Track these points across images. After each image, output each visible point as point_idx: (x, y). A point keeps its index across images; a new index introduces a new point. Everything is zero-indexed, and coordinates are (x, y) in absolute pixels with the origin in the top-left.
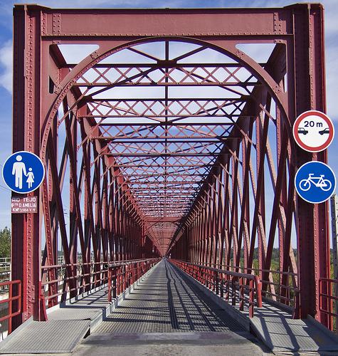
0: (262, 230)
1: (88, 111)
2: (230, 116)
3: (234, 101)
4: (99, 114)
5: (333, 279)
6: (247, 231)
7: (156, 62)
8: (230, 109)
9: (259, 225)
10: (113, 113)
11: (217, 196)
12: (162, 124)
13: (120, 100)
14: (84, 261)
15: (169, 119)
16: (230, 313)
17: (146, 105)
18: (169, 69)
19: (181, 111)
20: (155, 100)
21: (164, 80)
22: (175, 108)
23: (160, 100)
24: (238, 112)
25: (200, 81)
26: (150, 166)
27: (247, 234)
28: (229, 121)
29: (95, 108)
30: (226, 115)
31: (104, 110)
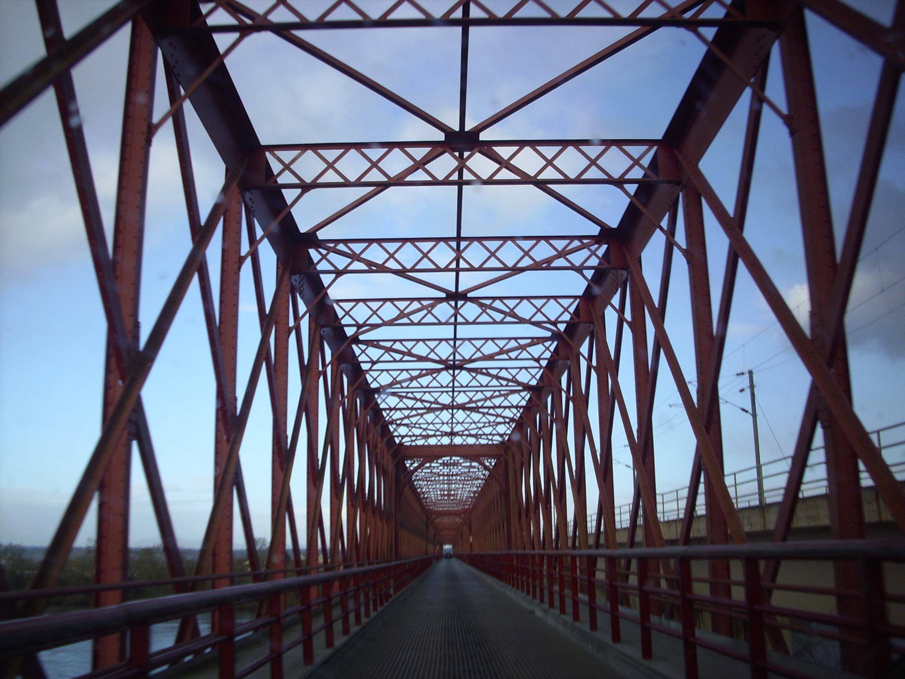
2: (537, 360)
10: (387, 357)
13: (370, 241)
20: (438, 240)
23: (446, 240)
24: (594, 262)
28: (536, 364)
29: (363, 351)
30: (534, 359)
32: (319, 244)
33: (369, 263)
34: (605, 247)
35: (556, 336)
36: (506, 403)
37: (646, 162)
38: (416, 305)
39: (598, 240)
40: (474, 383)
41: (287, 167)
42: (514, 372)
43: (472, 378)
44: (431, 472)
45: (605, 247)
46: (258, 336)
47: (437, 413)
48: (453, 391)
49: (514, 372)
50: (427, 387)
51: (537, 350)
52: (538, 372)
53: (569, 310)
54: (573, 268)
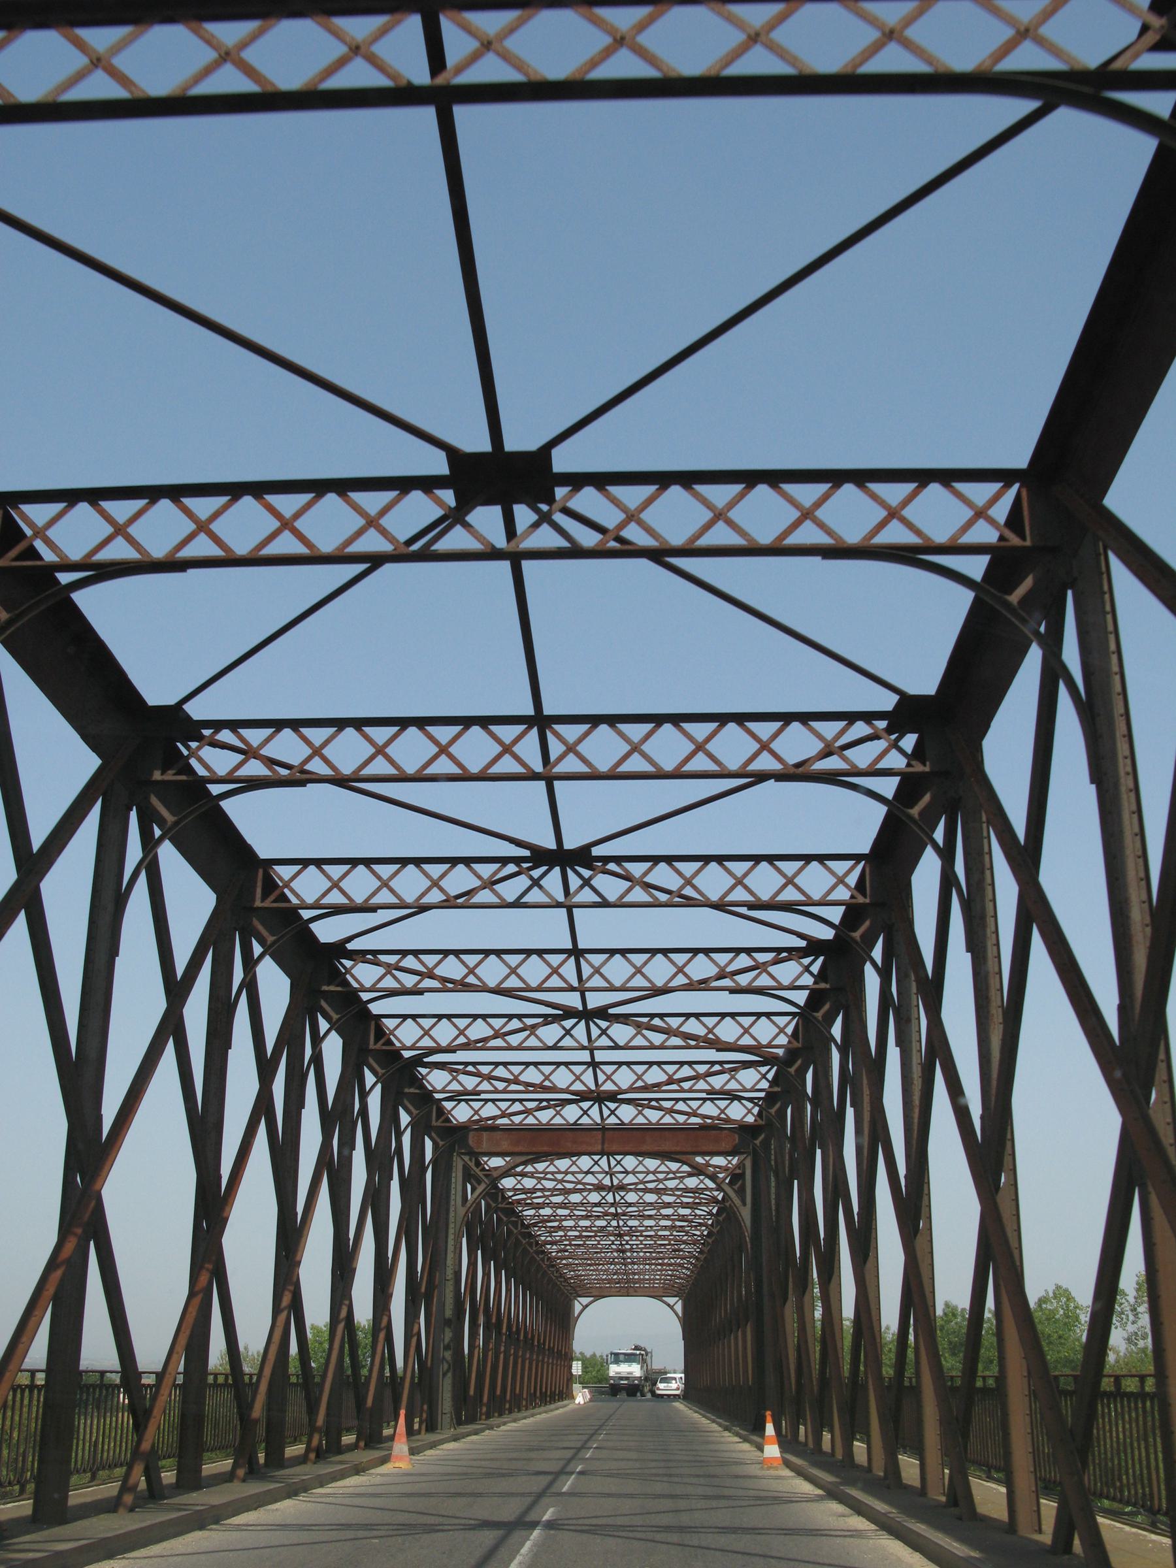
3: (783, 954)
13: (446, 953)
17: (456, 1026)
25: (664, 897)
32: (360, 956)
33: (444, 980)
37: (852, 880)
38: (515, 1024)
42: (639, 1041)
43: (638, 1162)
44: (565, 1236)
46: (319, 1138)
49: (639, 1041)
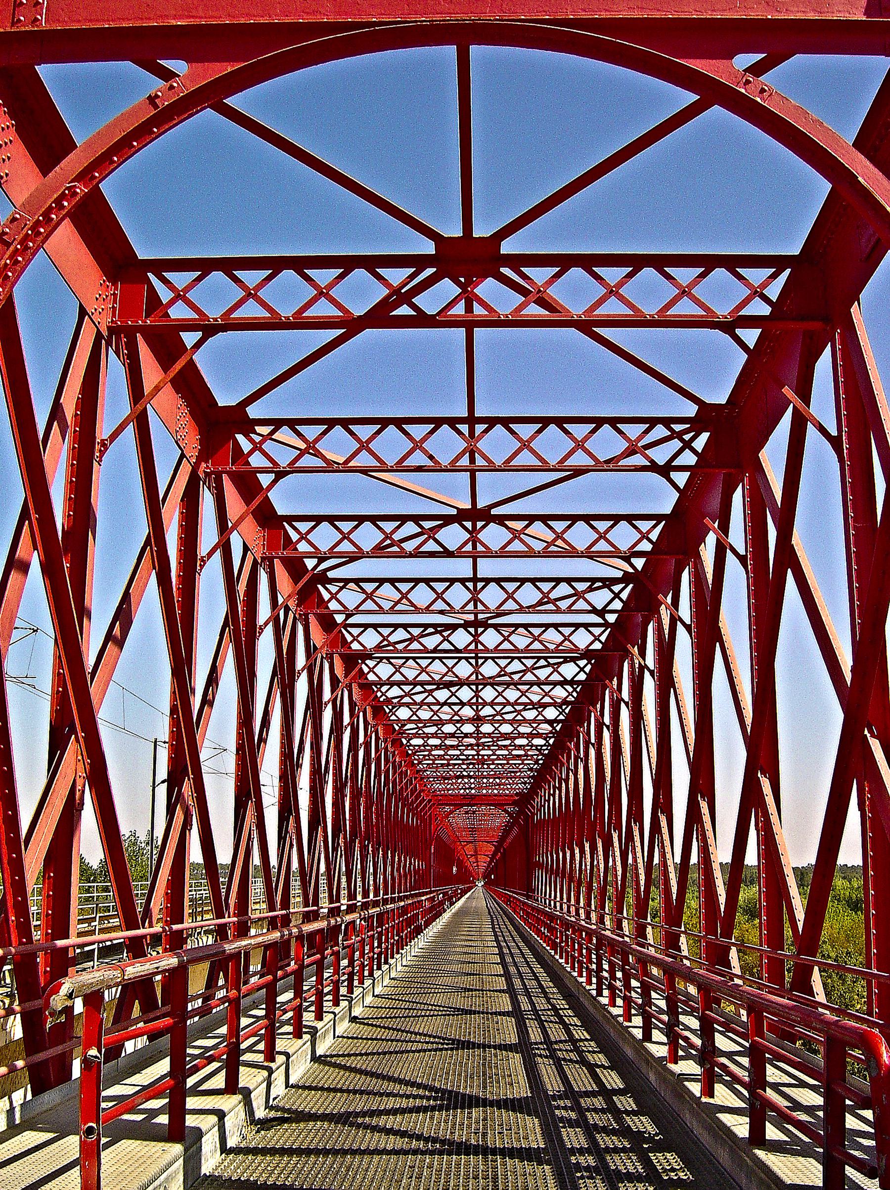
0: (667, 843)
1: (323, 603)
2: (601, 613)
3: (608, 583)
4: (340, 608)
5: (609, 928)
6: (638, 843)
7: (454, 512)
8: (600, 598)
9: (633, 840)
11: (592, 752)
12: (466, 625)
14: (331, 902)
15: (480, 616)
16: (567, 982)
18: (479, 524)
19: (509, 543)
21: (472, 604)
22: (492, 596)
24: (617, 605)
26: (445, 703)
27: (638, 849)
28: (599, 620)
30: (594, 611)
31: (351, 598)
34: (705, 437)
35: (553, 732)
36: (555, 677)
39: (697, 424)
40: (506, 646)
41: (179, 296)
45: (705, 437)
47: (453, 689)
48: (477, 658)
50: (460, 659)
51: (600, 598)
52: (654, 527)
53: (585, 669)
54: (653, 467)
